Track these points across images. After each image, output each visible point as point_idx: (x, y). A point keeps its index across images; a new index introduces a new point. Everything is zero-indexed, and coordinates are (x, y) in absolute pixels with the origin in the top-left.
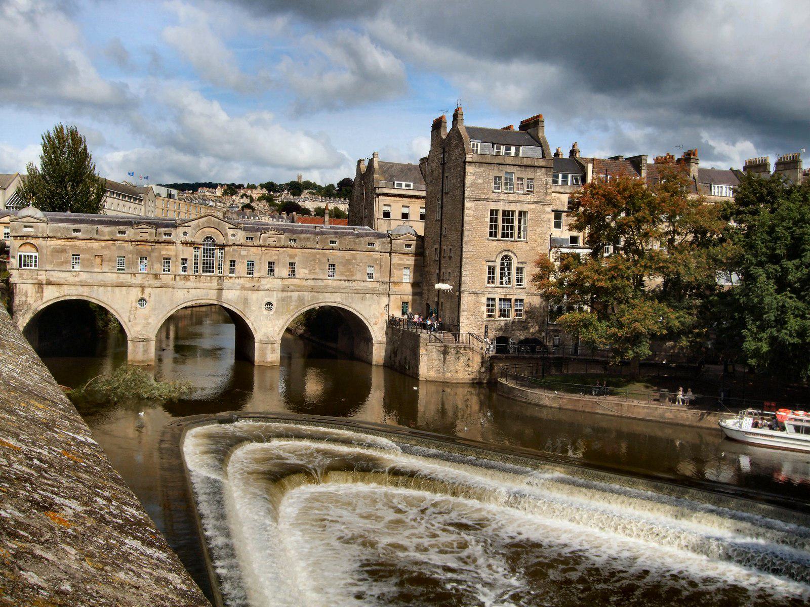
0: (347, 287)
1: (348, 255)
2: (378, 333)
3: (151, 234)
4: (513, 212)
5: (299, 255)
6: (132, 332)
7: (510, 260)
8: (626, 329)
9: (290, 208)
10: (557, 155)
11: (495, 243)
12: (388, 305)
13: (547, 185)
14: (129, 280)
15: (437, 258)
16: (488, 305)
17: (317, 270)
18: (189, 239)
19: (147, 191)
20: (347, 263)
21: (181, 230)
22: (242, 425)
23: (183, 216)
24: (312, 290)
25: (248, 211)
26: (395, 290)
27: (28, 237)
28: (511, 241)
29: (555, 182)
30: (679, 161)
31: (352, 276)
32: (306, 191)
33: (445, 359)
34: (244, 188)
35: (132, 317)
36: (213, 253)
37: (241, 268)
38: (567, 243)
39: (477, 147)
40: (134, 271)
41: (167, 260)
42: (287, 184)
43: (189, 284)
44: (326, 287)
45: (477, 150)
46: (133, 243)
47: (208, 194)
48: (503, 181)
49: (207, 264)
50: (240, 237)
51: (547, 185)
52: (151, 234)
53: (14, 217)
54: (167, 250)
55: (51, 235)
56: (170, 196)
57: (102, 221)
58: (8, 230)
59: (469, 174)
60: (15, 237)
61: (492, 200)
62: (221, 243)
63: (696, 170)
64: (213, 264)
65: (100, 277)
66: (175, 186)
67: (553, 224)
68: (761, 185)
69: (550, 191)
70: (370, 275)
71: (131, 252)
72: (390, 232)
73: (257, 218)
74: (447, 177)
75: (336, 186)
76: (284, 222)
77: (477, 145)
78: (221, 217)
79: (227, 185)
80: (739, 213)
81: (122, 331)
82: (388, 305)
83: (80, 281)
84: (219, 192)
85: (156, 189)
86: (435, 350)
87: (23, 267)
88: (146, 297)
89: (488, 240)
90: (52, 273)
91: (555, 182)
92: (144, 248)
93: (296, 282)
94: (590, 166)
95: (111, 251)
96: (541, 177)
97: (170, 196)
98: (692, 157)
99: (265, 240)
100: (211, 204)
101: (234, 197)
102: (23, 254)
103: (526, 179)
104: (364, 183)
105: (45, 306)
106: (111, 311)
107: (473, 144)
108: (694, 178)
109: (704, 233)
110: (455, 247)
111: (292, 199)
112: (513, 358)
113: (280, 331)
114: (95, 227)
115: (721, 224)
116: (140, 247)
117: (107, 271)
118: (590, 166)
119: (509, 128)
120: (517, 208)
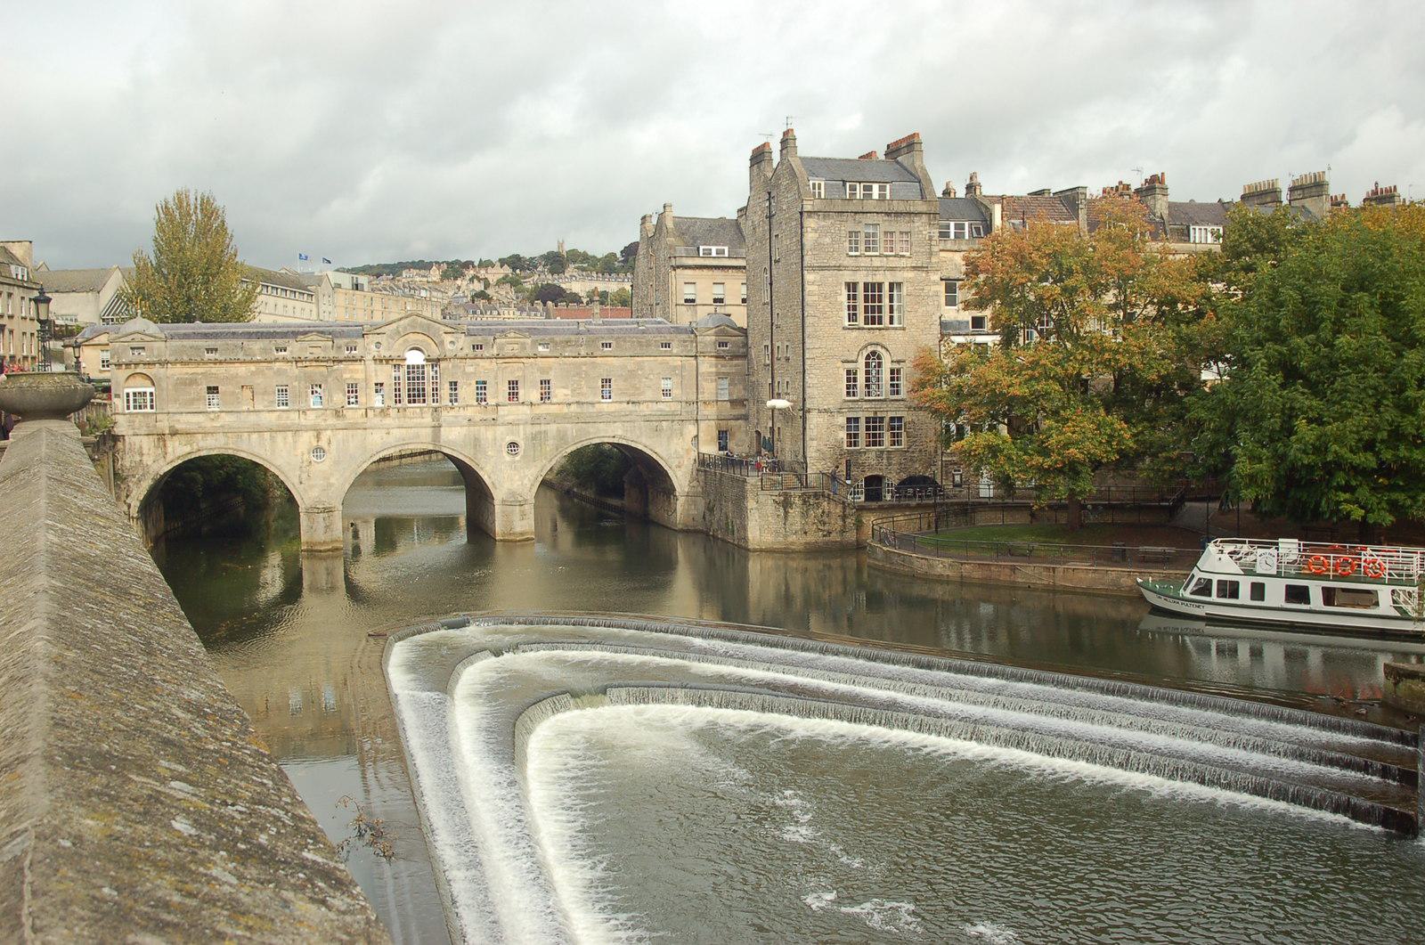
0: (631, 413)
1: (630, 363)
2: (681, 477)
3: (325, 349)
4: (880, 285)
5: (555, 369)
6: (303, 498)
7: (879, 357)
8: (1054, 457)
9: (551, 295)
10: (947, 193)
11: (855, 333)
12: (697, 436)
13: (930, 239)
14: (297, 421)
15: (768, 362)
16: (849, 428)
17: (585, 390)
18: (384, 353)
19: (319, 281)
20: (632, 374)
21: (371, 339)
22: (474, 632)
23: (378, 318)
24: (578, 419)
25: (481, 303)
26: (706, 413)
27: (137, 364)
28: (880, 329)
29: (944, 235)
30: (1138, 191)
31: (639, 395)
32: (572, 266)
33: (786, 513)
34: (474, 267)
35: (304, 476)
36: (423, 373)
37: (467, 392)
38: (967, 327)
39: (819, 188)
40: (303, 406)
41: (353, 389)
42: (543, 257)
43: (388, 421)
44: (600, 414)
45: (819, 193)
46: (299, 364)
47: (418, 279)
48: (862, 238)
49: (414, 389)
50: (464, 344)
51: (930, 239)
52: (325, 349)
53: (114, 336)
54: (351, 371)
55: (172, 359)
56: (357, 287)
57: (249, 333)
58: (106, 356)
59: (809, 230)
60: (119, 365)
61: (846, 268)
62: (434, 356)
63: (1165, 205)
64: (424, 390)
65: (253, 418)
66: (365, 270)
67: (943, 300)
68: (1259, 225)
69: (935, 249)
70: (666, 393)
71: (297, 378)
72: (694, 325)
73: (495, 313)
74: (777, 236)
75: (619, 255)
76: (536, 319)
77: (820, 185)
78: (439, 318)
79: (448, 263)
80: (1227, 267)
81: (291, 500)
82: (697, 436)
83: (222, 426)
84: (435, 274)
85: (335, 278)
86: (770, 502)
87: (132, 410)
88: (323, 443)
89: (485, 383)
90: (178, 417)
91: (944, 235)
92: (317, 370)
93: (553, 409)
94: (997, 210)
95: (268, 378)
96: (921, 229)
97: (357, 287)
98: (1157, 185)
99: (501, 348)
100: (423, 293)
101: (459, 282)
102: (131, 391)
103: (898, 234)
104: (653, 251)
105: (170, 467)
106: (272, 469)
107: (814, 184)
108: (1162, 218)
109: (1173, 303)
110: (793, 343)
111: (550, 279)
112: (892, 507)
113: (532, 485)
114: (239, 342)
115: (1197, 288)
116: (309, 369)
117: (261, 408)
118: (997, 210)
119: (869, 155)
120: (885, 279)
